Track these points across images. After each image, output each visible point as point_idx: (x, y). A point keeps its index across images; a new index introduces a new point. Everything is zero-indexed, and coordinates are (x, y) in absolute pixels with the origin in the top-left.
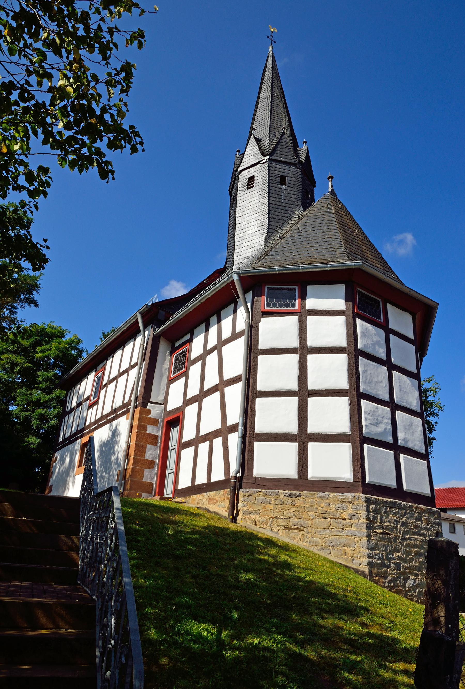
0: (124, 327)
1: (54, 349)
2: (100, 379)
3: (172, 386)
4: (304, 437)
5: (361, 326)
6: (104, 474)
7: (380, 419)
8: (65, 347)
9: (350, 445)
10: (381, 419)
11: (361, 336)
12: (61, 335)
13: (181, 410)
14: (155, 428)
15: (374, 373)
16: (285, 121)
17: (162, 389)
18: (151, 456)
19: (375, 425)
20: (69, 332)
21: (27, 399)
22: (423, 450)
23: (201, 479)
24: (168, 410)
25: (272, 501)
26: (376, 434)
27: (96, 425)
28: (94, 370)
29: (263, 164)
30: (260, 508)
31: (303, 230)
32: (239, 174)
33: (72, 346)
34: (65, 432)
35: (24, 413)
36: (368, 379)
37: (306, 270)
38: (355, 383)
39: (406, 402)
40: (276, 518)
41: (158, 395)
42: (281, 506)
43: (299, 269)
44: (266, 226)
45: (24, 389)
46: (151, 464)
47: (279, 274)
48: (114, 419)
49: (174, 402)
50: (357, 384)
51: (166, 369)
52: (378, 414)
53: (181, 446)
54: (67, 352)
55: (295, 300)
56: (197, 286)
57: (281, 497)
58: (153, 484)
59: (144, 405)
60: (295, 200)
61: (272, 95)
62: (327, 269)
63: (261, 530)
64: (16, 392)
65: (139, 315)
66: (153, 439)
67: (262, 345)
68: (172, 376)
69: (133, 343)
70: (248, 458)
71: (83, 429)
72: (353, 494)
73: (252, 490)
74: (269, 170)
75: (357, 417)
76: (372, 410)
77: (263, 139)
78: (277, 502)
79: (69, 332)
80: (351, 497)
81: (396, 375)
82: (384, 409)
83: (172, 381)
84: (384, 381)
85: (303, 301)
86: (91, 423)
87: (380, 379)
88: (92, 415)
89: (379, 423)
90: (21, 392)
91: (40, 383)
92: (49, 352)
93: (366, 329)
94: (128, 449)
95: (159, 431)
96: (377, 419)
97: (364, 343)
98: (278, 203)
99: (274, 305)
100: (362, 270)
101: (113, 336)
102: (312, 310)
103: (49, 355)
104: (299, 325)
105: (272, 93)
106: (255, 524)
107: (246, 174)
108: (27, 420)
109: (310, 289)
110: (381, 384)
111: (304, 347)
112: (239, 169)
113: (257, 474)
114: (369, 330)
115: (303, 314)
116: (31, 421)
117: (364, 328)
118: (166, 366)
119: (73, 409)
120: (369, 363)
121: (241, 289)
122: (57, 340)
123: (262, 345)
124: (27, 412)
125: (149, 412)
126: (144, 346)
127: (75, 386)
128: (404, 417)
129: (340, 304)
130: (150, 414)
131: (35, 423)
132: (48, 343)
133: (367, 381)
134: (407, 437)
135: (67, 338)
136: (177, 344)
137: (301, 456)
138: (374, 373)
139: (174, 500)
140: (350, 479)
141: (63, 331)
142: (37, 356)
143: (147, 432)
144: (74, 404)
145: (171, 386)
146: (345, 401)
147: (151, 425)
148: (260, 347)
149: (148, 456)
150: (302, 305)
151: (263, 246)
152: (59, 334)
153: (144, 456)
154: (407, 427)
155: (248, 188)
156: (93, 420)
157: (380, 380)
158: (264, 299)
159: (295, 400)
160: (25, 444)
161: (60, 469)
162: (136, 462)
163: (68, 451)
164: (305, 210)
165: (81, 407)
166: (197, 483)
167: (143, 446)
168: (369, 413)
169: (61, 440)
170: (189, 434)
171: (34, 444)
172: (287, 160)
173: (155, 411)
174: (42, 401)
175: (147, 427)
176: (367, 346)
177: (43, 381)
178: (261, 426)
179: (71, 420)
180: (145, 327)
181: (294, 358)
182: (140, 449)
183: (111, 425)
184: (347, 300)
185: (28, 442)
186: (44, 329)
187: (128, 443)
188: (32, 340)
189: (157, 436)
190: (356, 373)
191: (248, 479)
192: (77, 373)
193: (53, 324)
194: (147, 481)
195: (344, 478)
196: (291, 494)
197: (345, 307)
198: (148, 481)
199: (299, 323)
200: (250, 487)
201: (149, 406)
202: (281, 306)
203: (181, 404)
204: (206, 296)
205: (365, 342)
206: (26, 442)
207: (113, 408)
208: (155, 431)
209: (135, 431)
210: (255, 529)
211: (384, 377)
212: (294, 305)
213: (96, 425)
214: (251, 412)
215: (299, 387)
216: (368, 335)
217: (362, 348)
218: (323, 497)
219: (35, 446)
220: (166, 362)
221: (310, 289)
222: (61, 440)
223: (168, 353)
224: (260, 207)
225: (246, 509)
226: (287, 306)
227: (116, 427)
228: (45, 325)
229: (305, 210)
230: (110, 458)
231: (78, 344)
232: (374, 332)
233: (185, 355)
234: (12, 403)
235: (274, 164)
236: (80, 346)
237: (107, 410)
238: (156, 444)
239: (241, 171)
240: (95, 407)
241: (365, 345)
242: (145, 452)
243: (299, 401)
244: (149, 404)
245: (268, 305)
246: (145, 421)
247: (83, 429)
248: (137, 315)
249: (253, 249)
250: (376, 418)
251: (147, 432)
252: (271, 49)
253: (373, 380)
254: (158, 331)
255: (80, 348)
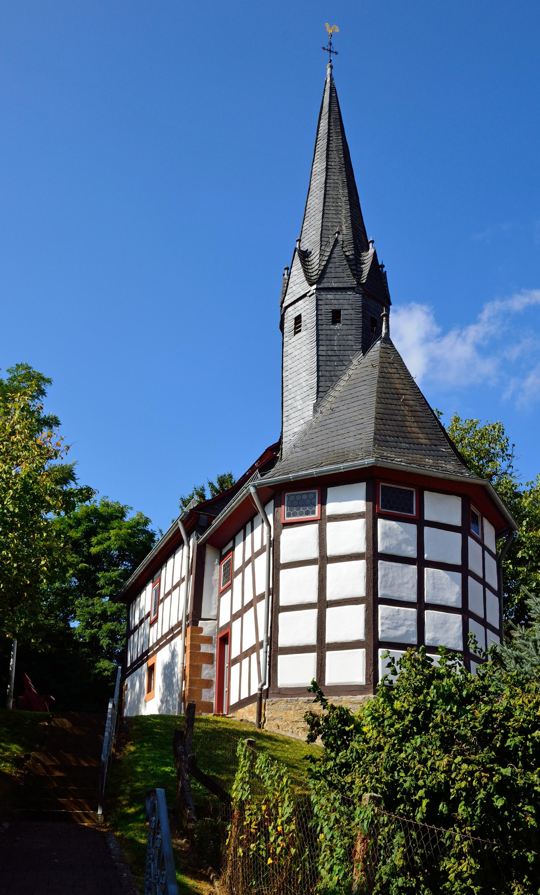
0: (168, 535)
1: (113, 538)
2: (157, 591)
3: (222, 599)
4: (323, 647)
5: (382, 527)
6: (169, 698)
7: (401, 622)
8: (128, 533)
9: (364, 651)
10: (402, 621)
11: (383, 538)
12: (120, 515)
13: (229, 626)
14: (209, 646)
15: (398, 575)
16: (344, 212)
17: (213, 603)
18: (208, 676)
19: (393, 629)
20: (131, 508)
21: (90, 612)
22: (459, 647)
23: (245, 695)
24: (220, 626)
25: (293, 708)
26: (394, 637)
27: (158, 646)
28: (151, 580)
29: (310, 296)
30: (282, 714)
31: (337, 410)
32: (285, 312)
33: (138, 530)
34: (132, 655)
35: (88, 631)
36: (389, 583)
37: (319, 475)
38: (372, 590)
39: (441, 600)
40: (296, 721)
41: (211, 609)
42: (300, 711)
43: (313, 474)
44: (315, 389)
45: (84, 598)
46: (208, 684)
47: (295, 481)
48: (172, 639)
49: (224, 619)
50: (374, 590)
51: (216, 580)
52: (398, 617)
53: (231, 663)
54: (132, 540)
55: (315, 506)
56: (249, 469)
57: (300, 703)
58: (212, 703)
59: (195, 623)
60: (352, 343)
61: (327, 169)
62: (341, 471)
63: (283, 733)
64: (74, 604)
65: (180, 522)
66: (209, 658)
67: (282, 561)
68: (222, 588)
69: (181, 551)
70: (273, 670)
71: (148, 651)
72: (363, 696)
73: (275, 700)
74: (317, 305)
75: (372, 623)
76: (391, 614)
77: (313, 253)
78: (297, 708)
79: (131, 508)
80: (361, 699)
81: (429, 573)
82: (408, 611)
83: (222, 593)
84: (411, 582)
85: (323, 506)
86: (154, 644)
87: (405, 580)
88: (155, 634)
89: (400, 626)
90: (80, 604)
91: (103, 587)
92: (108, 543)
93: (390, 528)
94: (185, 670)
95: (211, 651)
96: (397, 623)
97: (385, 545)
98: (330, 353)
99: (295, 515)
100: (379, 467)
101: (161, 544)
102: (332, 515)
103: (109, 547)
104: (319, 533)
105: (327, 161)
106: (279, 728)
107: (293, 312)
108: (95, 639)
109: (331, 491)
110: (406, 586)
111: (324, 557)
112: (284, 305)
113: (281, 685)
114: (394, 529)
115: (322, 521)
116: (100, 640)
117: (387, 527)
118: (216, 576)
119: (137, 628)
120: (392, 565)
121: (259, 503)
122: (115, 523)
123: (282, 561)
124: (92, 629)
125: (201, 630)
126: (189, 557)
127: (135, 599)
128: (436, 616)
129: (360, 505)
130: (202, 632)
131: (105, 642)
132: (106, 529)
133: (388, 585)
134: (437, 636)
135: (130, 517)
136: (224, 551)
137: (320, 665)
138: (398, 575)
139: (228, 716)
140: (362, 683)
141: (122, 508)
142: (93, 550)
143: (201, 651)
144: (137, 621)
145: (221, 599)
146: (361, 608)
147: (205, 643)
148: (282, 561)
149: (205, 676)
150: (323, 511)
151: (311, 418)
152: (117, 514)
153: (201, 676)
154: (439, 626)
155: (296, 333)
156: (155, 641)
157: (406, 582)
158: (284, 509)
159: (314, 612)
160: (97, 671)
161: (131, 697)
162: (192, 683)
163: (137, 675)
164: (364, 353)
165: (143, 624)
166: (242, 698)
167: (198, 666)
168: (387, 618)
169: (129, 665)
170: (235, 652)
171: (108, 670)
172: (341, 285)
173: (207, 628)
174: (109, 613)
175: (200, 647)
176: (390, 548)
177: (107, 584)
178: (283, 641)
179: (136, 639)
180: (189, 536)
181: (314, 569)
182: (195, 669)
183: (170, 645)
184: (367, 500)
185: (100, 668)
186: (96, 509)
187: (183, 664)
188: (82, 528)
189: (212, 655)
190: (374, 579)
191: (274, 690)
192: (133, 584)
193: (106, 501)
194: (205, 701)
195: (357, 682)
196: (308, 700)
197: (365, 508)
198: (207, 700)
199: (319, 531)
200: (274, 697)
201: (201, 623)
202: (301, 515)
203: (229, 620)
204: (233, 507)
205: (387, 543)
206: (98, 669)
207: (171, 627)
208: (209, 649)
209: (188, 651)
210: (279, 733)
211: (411, 578)
212: (314, 513)
213: (158, 646)
214: (275, 627)
215: (318, 598)
216: (394, 534)
217: (383, 550)
218: (337, 700)
219: (109, 673)
220: (214, 574)
221: (331, 491)
222: (129, 665)
223: (217, 562)
224: (308, 362)
225: (270, 716)
226: (307, 513)
227: (174, 647)
228: (96, 504)
229: (364, 353)
230: (172, 681)
231: (146, 525)
232: (401, 529)
233: (230, 564)
234: (72, 618)
235: (324, 295)
236: (149, 528)
237: (166, 630)
238: (212, 663)
239: (287, 307)
240: (156, 625)
241: (387, 547)
242: (201, 672)
243: (318, 613)
244: (200, 622)
245: (289, 515)
246: (196, 640)
247: (148, 651)
248: (178, 523)
249: (302, 422)
250: (395, 621)
251: (201, 651)
252: (329, 69)
253: (396, 583)
254: (202, 538)
255: (149, 530)
